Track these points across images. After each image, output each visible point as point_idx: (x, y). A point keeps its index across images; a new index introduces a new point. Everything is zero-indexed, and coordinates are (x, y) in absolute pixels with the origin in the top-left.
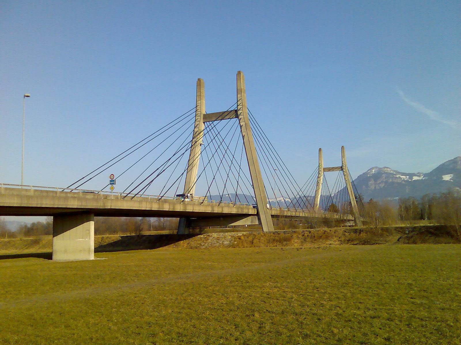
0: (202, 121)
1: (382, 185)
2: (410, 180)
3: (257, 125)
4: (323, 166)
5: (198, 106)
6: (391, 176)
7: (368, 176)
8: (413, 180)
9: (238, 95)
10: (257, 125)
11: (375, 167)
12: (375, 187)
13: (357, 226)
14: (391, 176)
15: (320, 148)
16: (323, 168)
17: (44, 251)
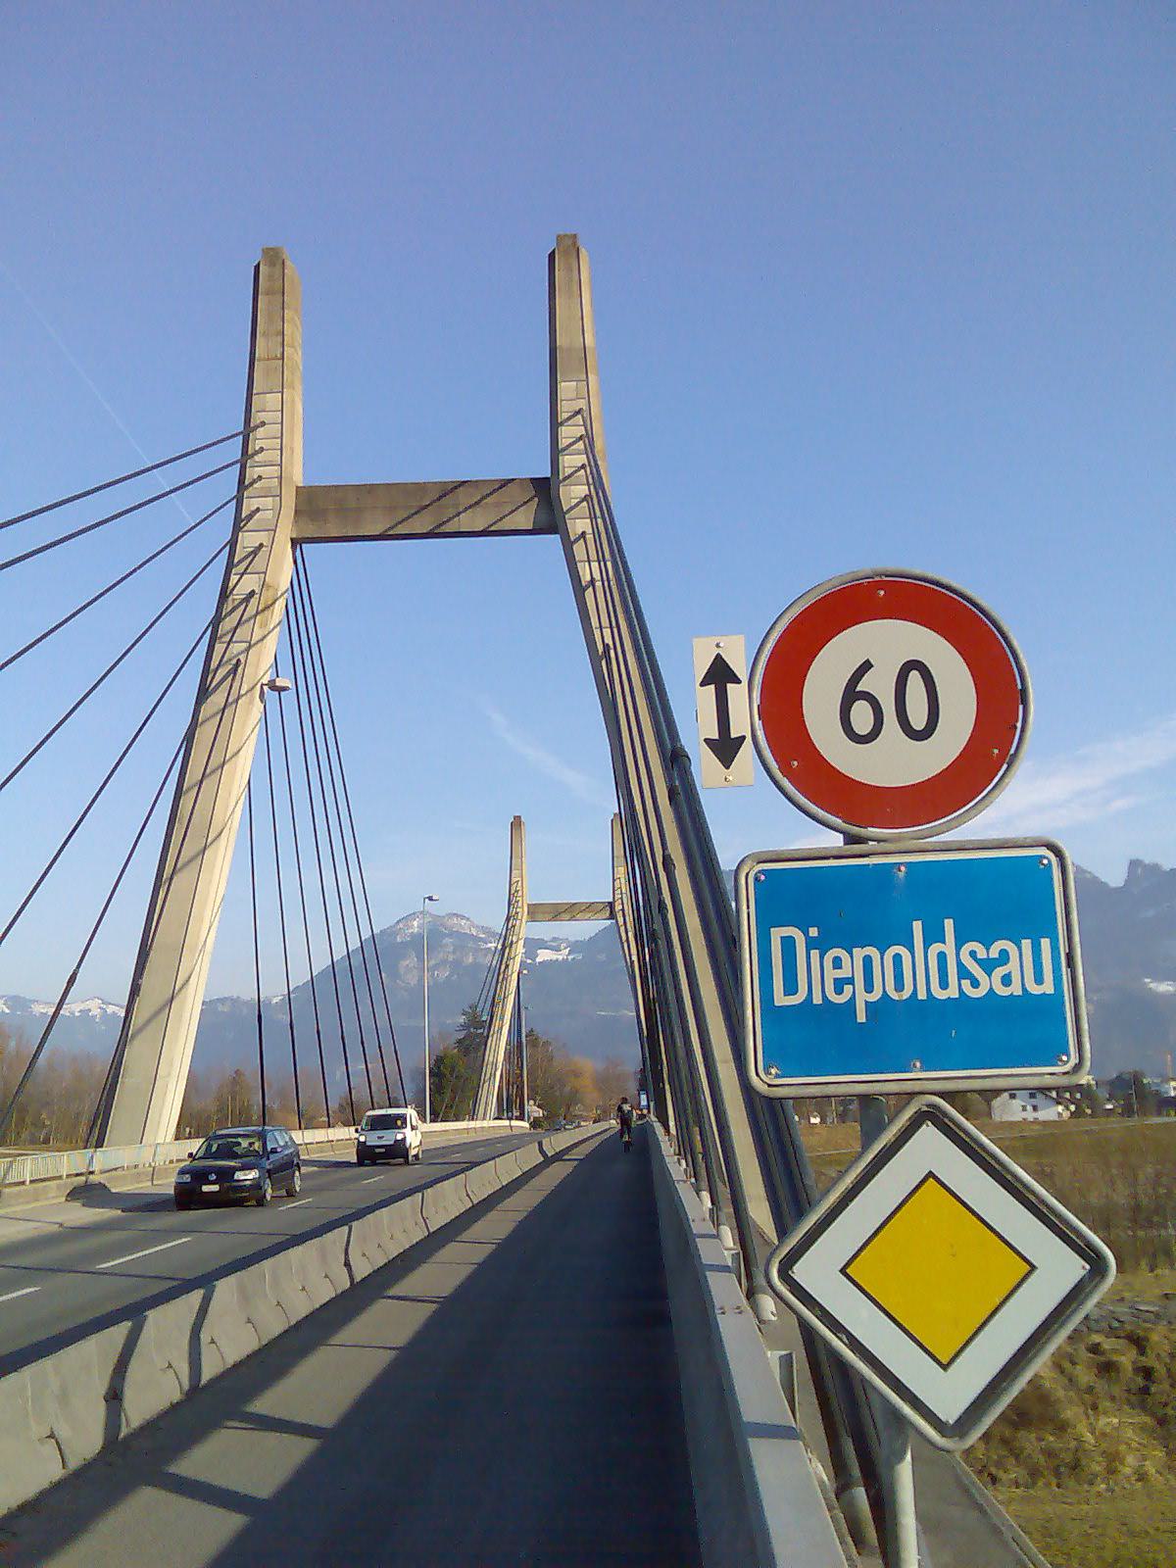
0: (286, 532)
1: (443, 974)
2: (529, 961)
3: (322, 692)
4: (528, 897)
5: (263, 424)
6: (471, 944)
7: (399, 940)
8: (538, 960)
9: (562, 386)
10: (322, 692)
13: (572, 1119)
16: (528, 905)
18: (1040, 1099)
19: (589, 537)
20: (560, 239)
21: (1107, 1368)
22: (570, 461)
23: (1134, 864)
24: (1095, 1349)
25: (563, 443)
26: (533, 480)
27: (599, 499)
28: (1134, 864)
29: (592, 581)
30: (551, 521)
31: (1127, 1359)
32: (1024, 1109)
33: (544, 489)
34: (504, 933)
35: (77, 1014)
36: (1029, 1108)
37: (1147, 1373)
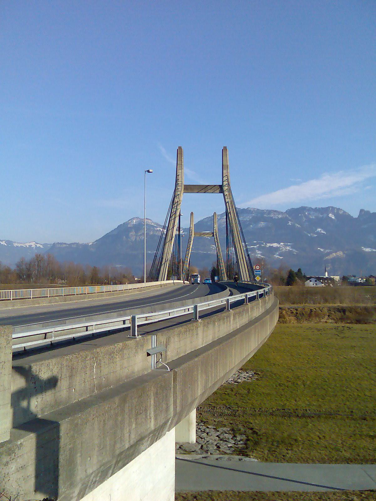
6: (152, 228)
7: (129, 226)
9: (224, 171)
11: (136, 218)
12: (136, 239)
14: (152, 228)
15: (192, 212)
17: (70, 337)
18: (318, 282)
19: (228, 195)
20: (224, 147)
21: (292, 313)
22: (225, 183)
23: (362, 211)
24: (291, 311)
25: (224, 180)
26: (219, 185)
27: (230, 190)
28: (362, 211)
29: (228, 202)
30: (222, 191)
31: (295, 312)
32: (313, 284)
33: (221, 187)
34: (167, 225)
35: (28, 247)
36: (315, 284)
37: (297, 313)
